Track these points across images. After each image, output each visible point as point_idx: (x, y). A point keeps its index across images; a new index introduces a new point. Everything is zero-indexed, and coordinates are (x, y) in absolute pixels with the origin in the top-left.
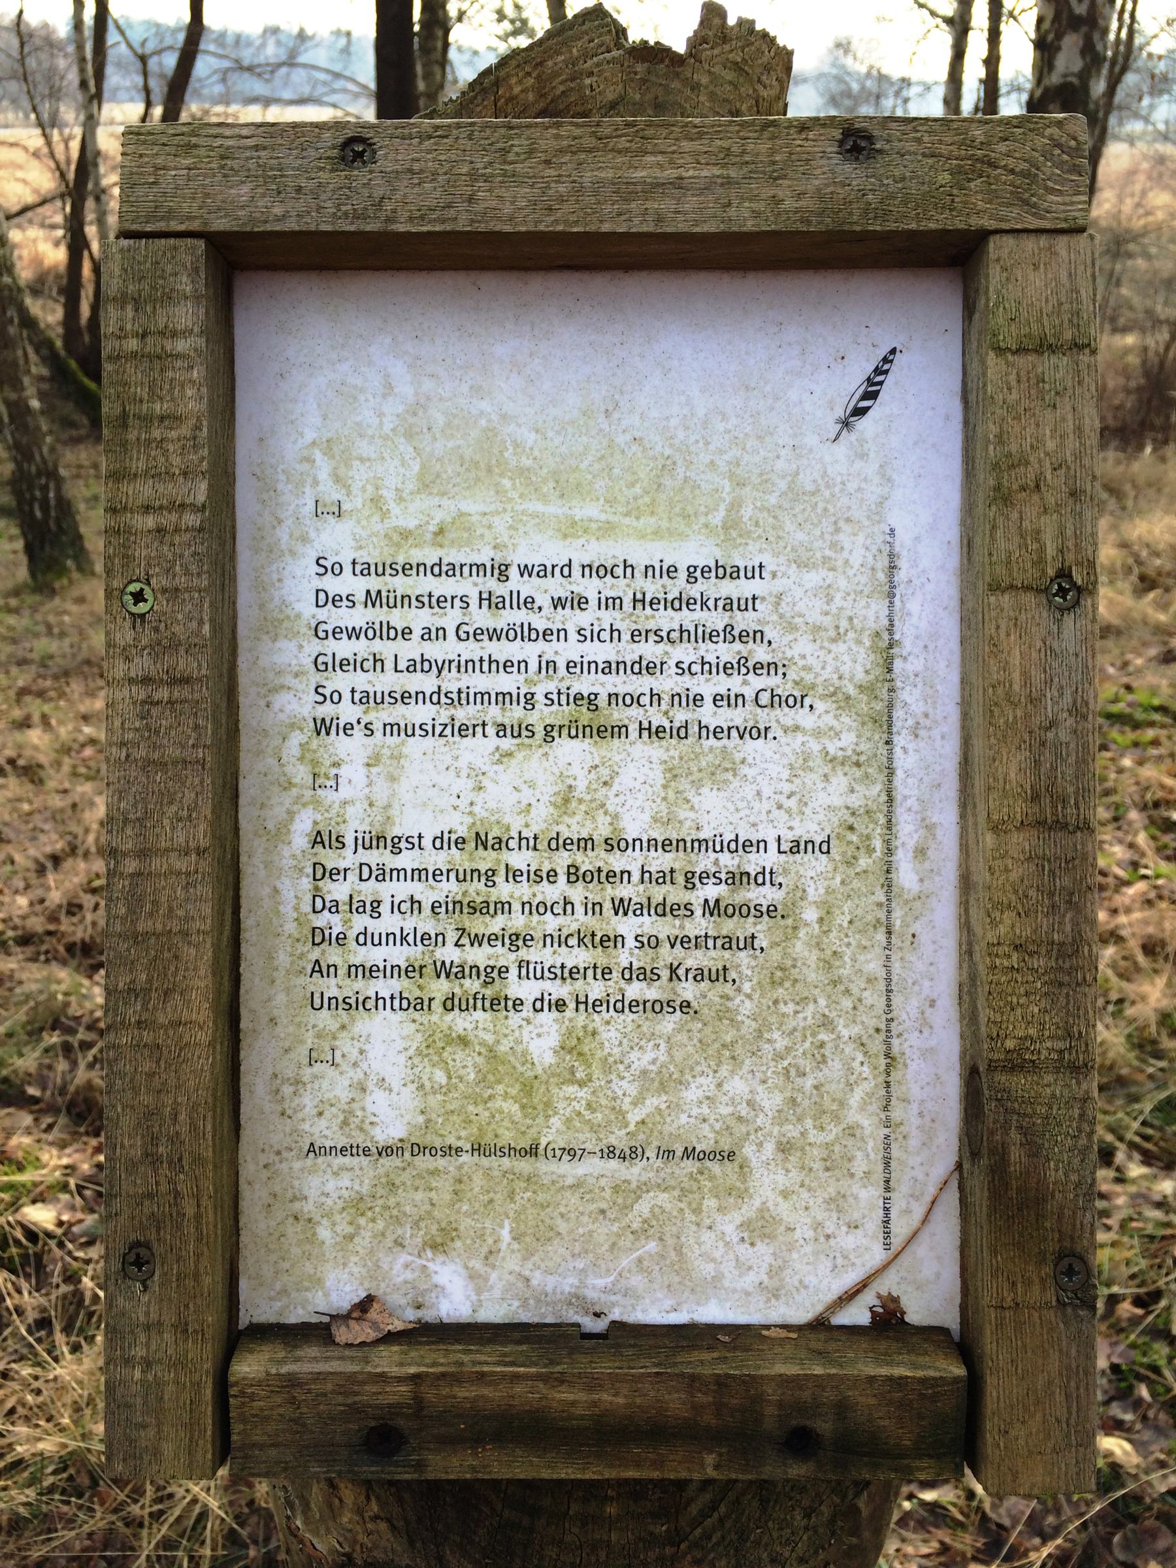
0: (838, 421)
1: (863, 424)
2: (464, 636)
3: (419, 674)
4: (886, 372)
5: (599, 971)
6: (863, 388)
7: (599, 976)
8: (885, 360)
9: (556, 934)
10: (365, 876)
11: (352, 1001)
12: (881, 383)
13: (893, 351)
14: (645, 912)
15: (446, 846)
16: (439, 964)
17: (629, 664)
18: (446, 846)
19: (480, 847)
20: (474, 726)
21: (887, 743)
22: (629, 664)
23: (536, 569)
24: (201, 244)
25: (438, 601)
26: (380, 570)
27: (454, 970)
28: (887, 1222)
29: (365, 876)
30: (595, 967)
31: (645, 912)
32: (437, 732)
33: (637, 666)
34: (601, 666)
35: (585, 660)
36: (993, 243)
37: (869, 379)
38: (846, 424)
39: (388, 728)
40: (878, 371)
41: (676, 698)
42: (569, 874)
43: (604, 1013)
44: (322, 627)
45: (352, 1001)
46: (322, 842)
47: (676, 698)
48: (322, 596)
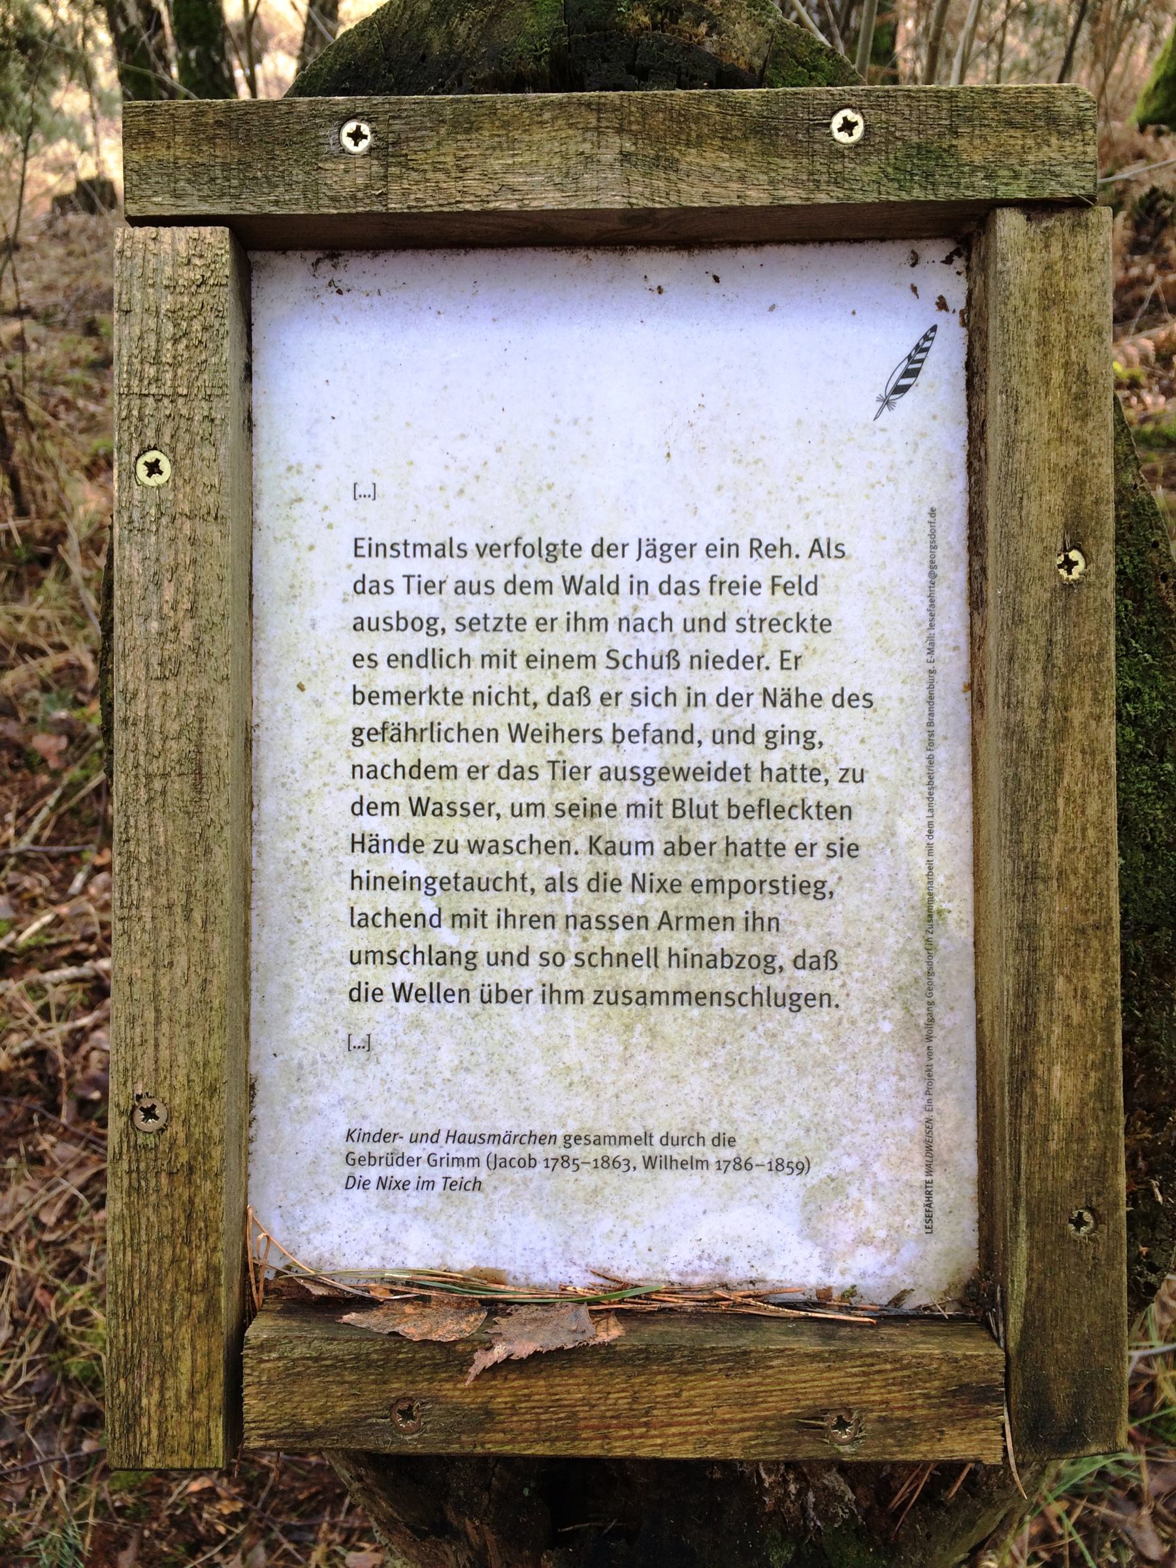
0: (878, 400)
3: (719, 970)
4: (927, 350)
8: (926, 338)
11: (837, 848)
12: (921, 361)
15: (601, 887)
16: (514, 728)
17: (712, 622)
18: (601, 887)
21: (935, 547)
22: (712, 622)
23: (487, 846)
24: (223, 232)
26: (475, 589)
27: (431, 807)
28: (929, 1205)
30: (509, 618)
32: (850, 773)
33: (415, 770)
34: (434, 549)
37: (909, 357)
38: (887, 402)
40: (919, 349)
41: (479, 696)
42: (675, 808)
43: (704, 895)
45: (837, 848)
46: (669, 923)
47: (479, 696)
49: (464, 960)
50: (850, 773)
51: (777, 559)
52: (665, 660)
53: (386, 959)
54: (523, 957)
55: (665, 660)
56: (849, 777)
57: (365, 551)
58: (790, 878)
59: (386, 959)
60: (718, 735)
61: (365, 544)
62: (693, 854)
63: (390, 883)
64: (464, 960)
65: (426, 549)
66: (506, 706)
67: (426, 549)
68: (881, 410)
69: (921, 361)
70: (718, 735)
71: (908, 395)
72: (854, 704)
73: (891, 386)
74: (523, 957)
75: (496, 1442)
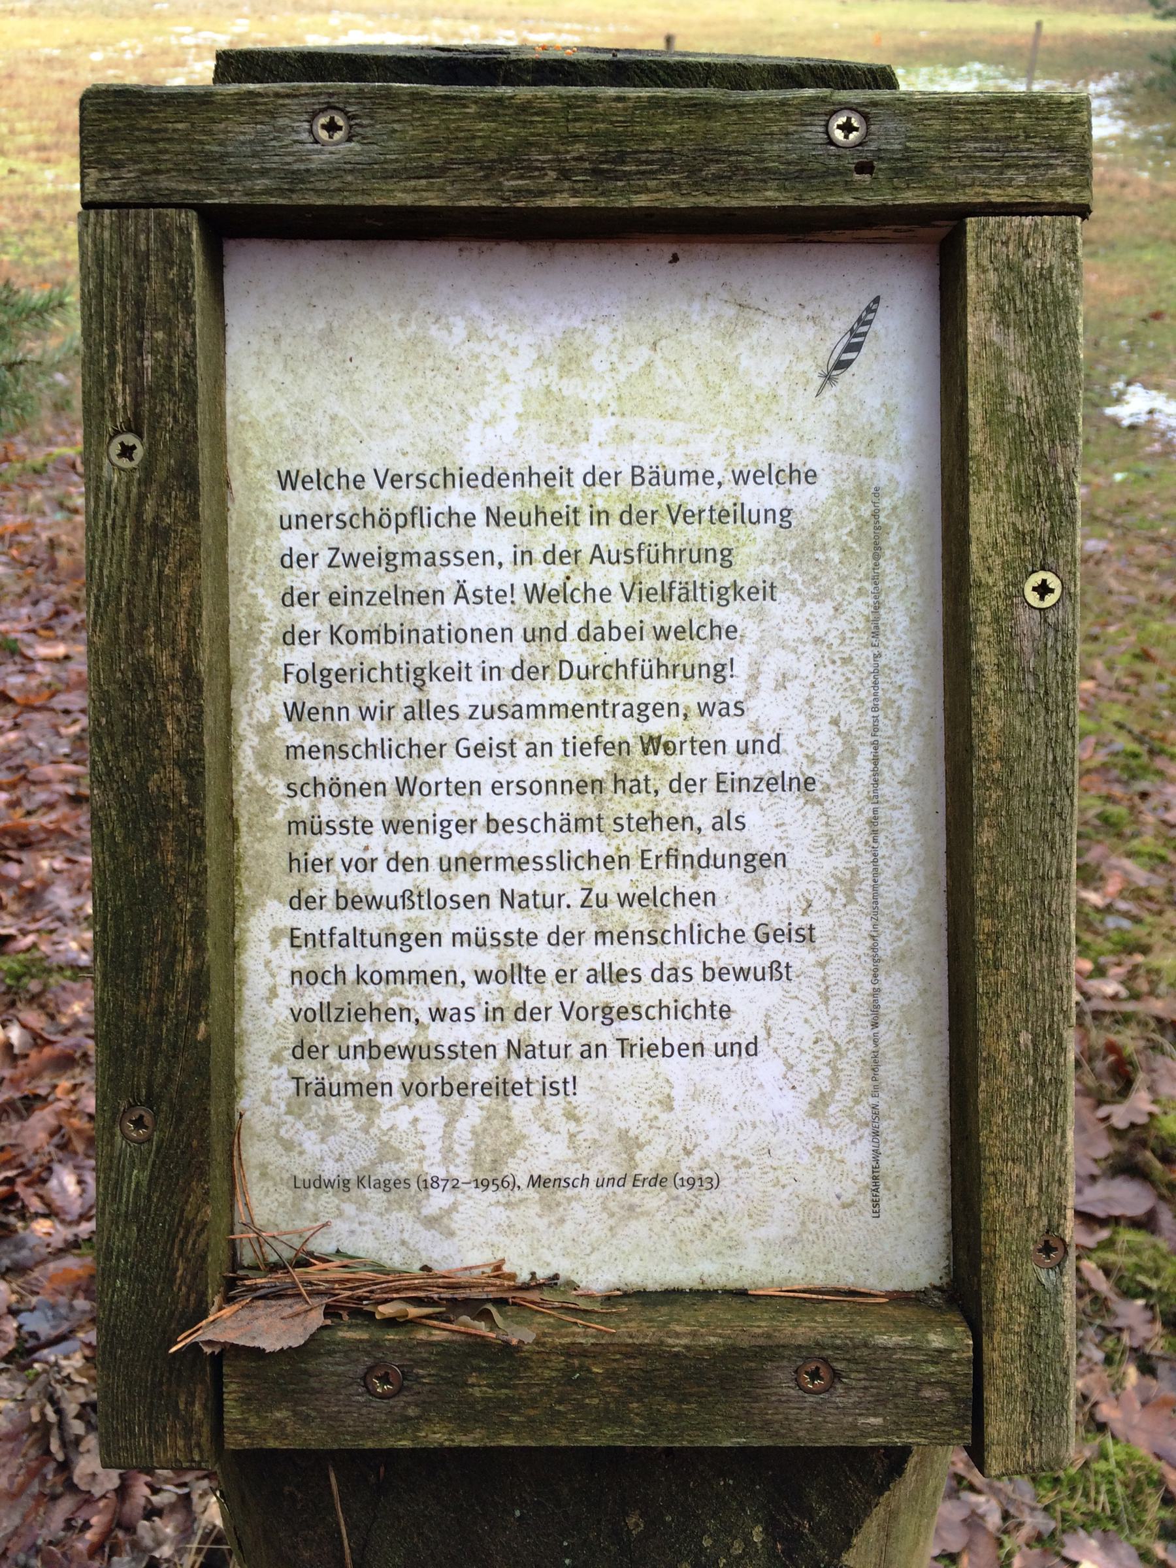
1: (845, 377)
2: (464, 752)
4: (870, 322)
5: (696, 745)
6: (845, 340)
7: (697, 751)
8: (869, 310)
9: (431, 821)
10: (566, 673)
12: (864, 334)
13: (877, 300)
14: (600, 979)
19: (513, 1056)
20: (487, 859)
25: (456, 788)
29: (566, 673)
31: (600, 979)
32: (480, 709)
35: (349, 589)
36: (972, 223)
37: (852, 330)
38: (828, 378)
39: (458, 937)
40: (861, 321)
42: (634, 476)
44: (463, 744)
46: (465, 597)
48: (566, 666)
49: (743, 862)
50: (480, 709)
51: (731, 526)
52: (400, 901)
53: (647, 939)
54: (752, 1046)
55: (400, 901)
56: (479, 713)
57: (651, 863)
58: (707, 584)
59: (647, 939)
60: (445, 863)
61: (652, 855)
62: (295, 565)
63: (313, 521)
64: (743, 862)
65: (415, 558)
66: (441, 490)
67: (415, 558)
68: (822, 386)
69: (864, 334)
70: (445, 863)
71: (853, 368)
72: (508, 829)
73: (832, 362)
74: (752, 1046)
75: (244, 133)
